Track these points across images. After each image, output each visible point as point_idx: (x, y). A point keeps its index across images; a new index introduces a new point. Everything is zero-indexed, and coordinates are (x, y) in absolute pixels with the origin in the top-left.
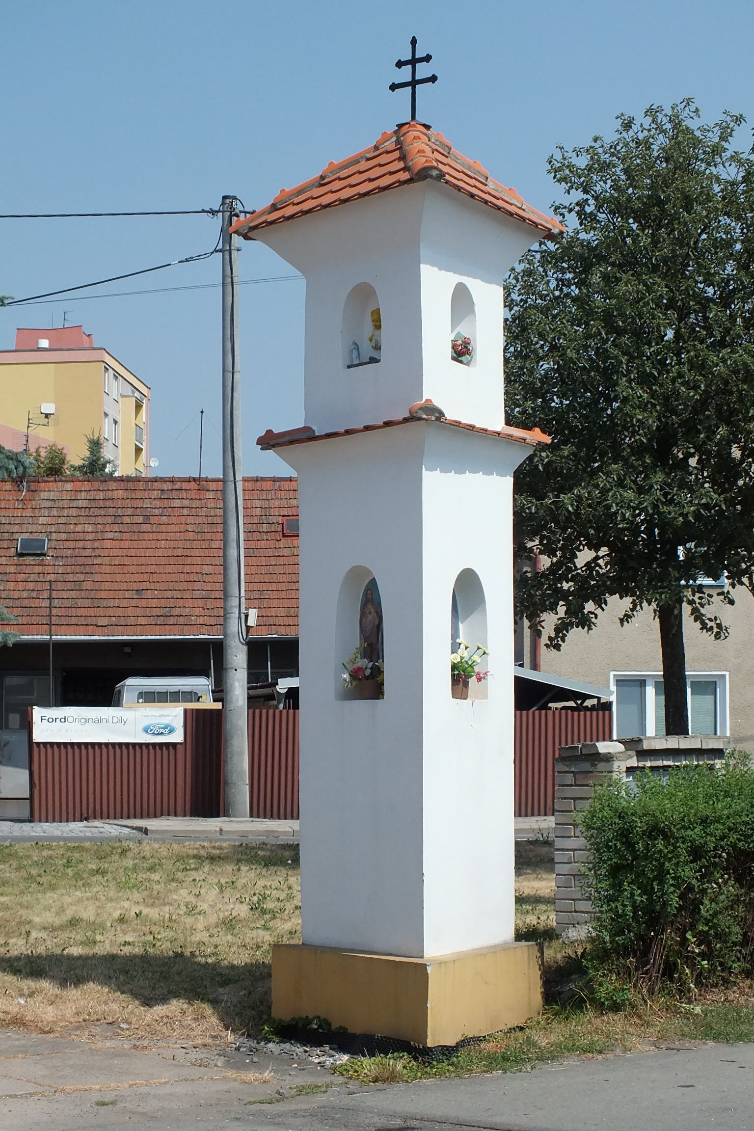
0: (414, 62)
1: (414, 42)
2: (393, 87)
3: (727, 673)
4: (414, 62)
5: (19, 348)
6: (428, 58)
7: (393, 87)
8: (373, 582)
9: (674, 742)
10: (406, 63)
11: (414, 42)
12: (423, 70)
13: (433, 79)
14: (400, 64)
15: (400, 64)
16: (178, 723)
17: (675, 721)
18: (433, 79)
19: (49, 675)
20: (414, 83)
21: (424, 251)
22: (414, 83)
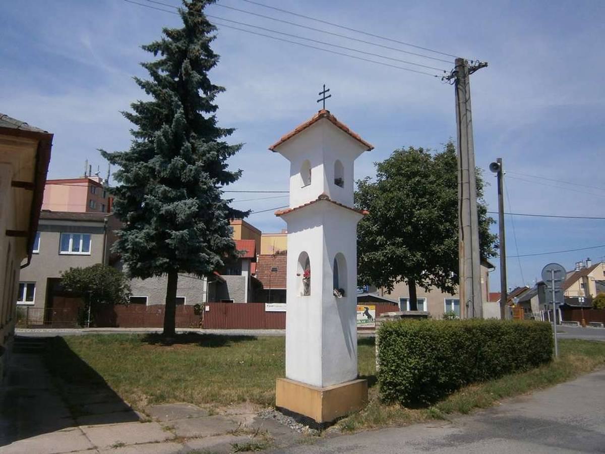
0: (324, 92)
1: (324, 86)
2: (318, 101)
3: (89, 253)
4: (324, 92)
5: (234, 23)
6: (328, 90)
7: (318, 101)
8: (308, 258)
9: (413, 313)
10: (322, 93)
11: (324, 86)
12: (327, 94)
13: (330, 96)
14: (320, 94)
15: (320, 94)
16: (242, 274)
17: (413, 307)
18: (330, 96)
19: (557, 339)
20: (324, 99)
21: (243, 268)
22: (324, 99)
